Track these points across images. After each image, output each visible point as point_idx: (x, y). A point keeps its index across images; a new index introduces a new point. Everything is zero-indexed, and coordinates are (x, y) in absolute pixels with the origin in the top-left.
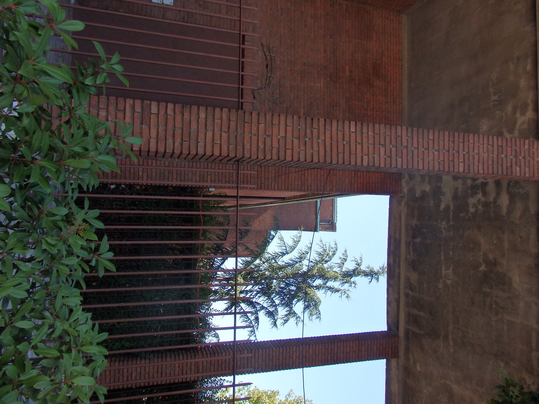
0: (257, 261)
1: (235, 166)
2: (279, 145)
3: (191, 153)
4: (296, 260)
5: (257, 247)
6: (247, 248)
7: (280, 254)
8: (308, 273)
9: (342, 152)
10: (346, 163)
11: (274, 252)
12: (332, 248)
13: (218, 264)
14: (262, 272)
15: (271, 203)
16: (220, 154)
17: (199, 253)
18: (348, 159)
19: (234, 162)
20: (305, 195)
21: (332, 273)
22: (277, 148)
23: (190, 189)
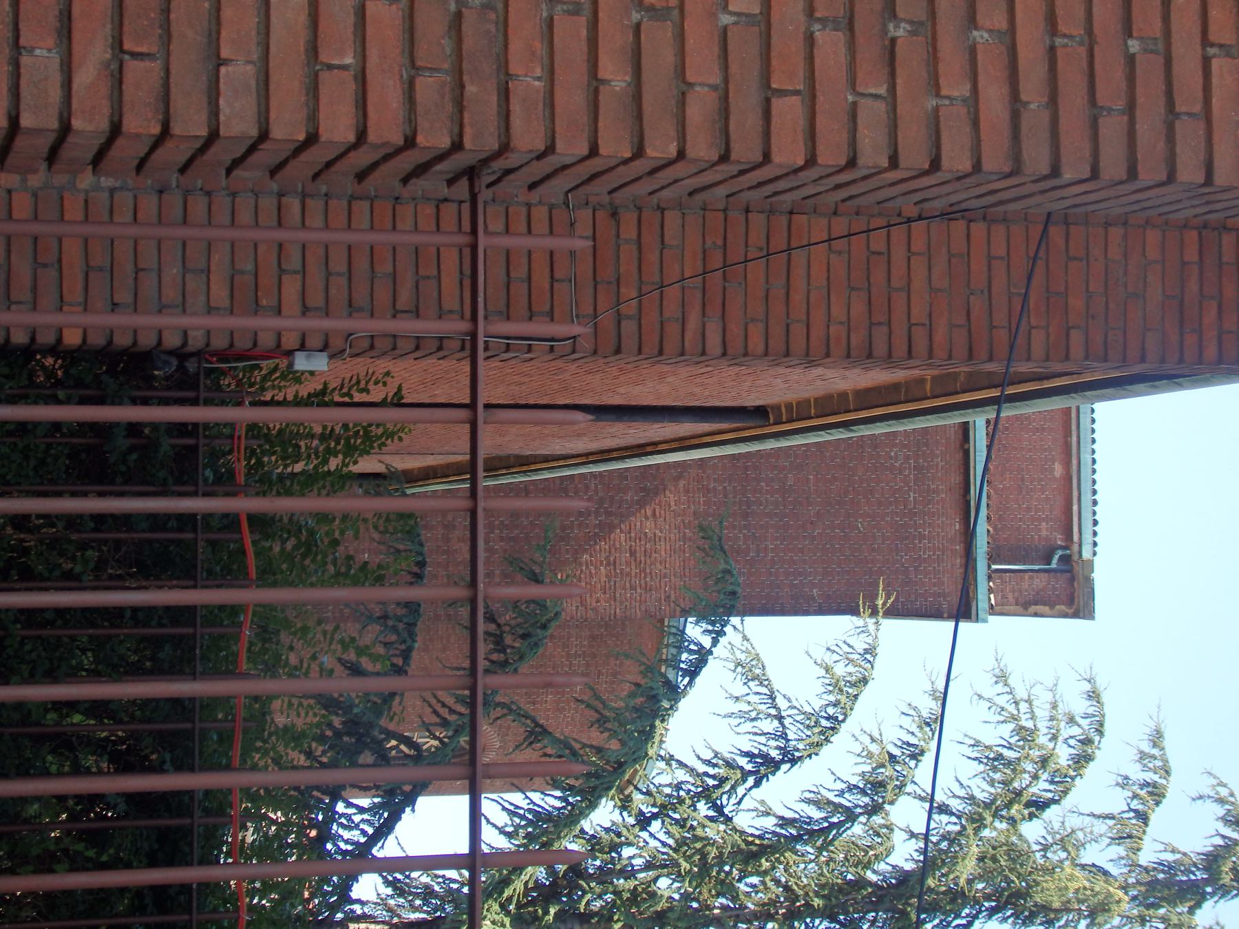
0: (604, 815)
1: (450, 210)
2: (726, 68)
3: (177, 129)
4: (847, 800)
5: (601, 721)
6: (537, 733)
7: (743, 762)
8: (922, 881)
9: (1120, 105)
10: (1150, 172)
11: (708, 755)
12: (1071, 720)
13: (355, 835)
14: (631, 884)
15: (683, 444)
16: (362, 136)
17: (237, 762)
18: (1161, 145)
19: (451, 182)
20: (895, 387)
21: (1071, 878)
22: (714, 88)
23: (175, 362)
